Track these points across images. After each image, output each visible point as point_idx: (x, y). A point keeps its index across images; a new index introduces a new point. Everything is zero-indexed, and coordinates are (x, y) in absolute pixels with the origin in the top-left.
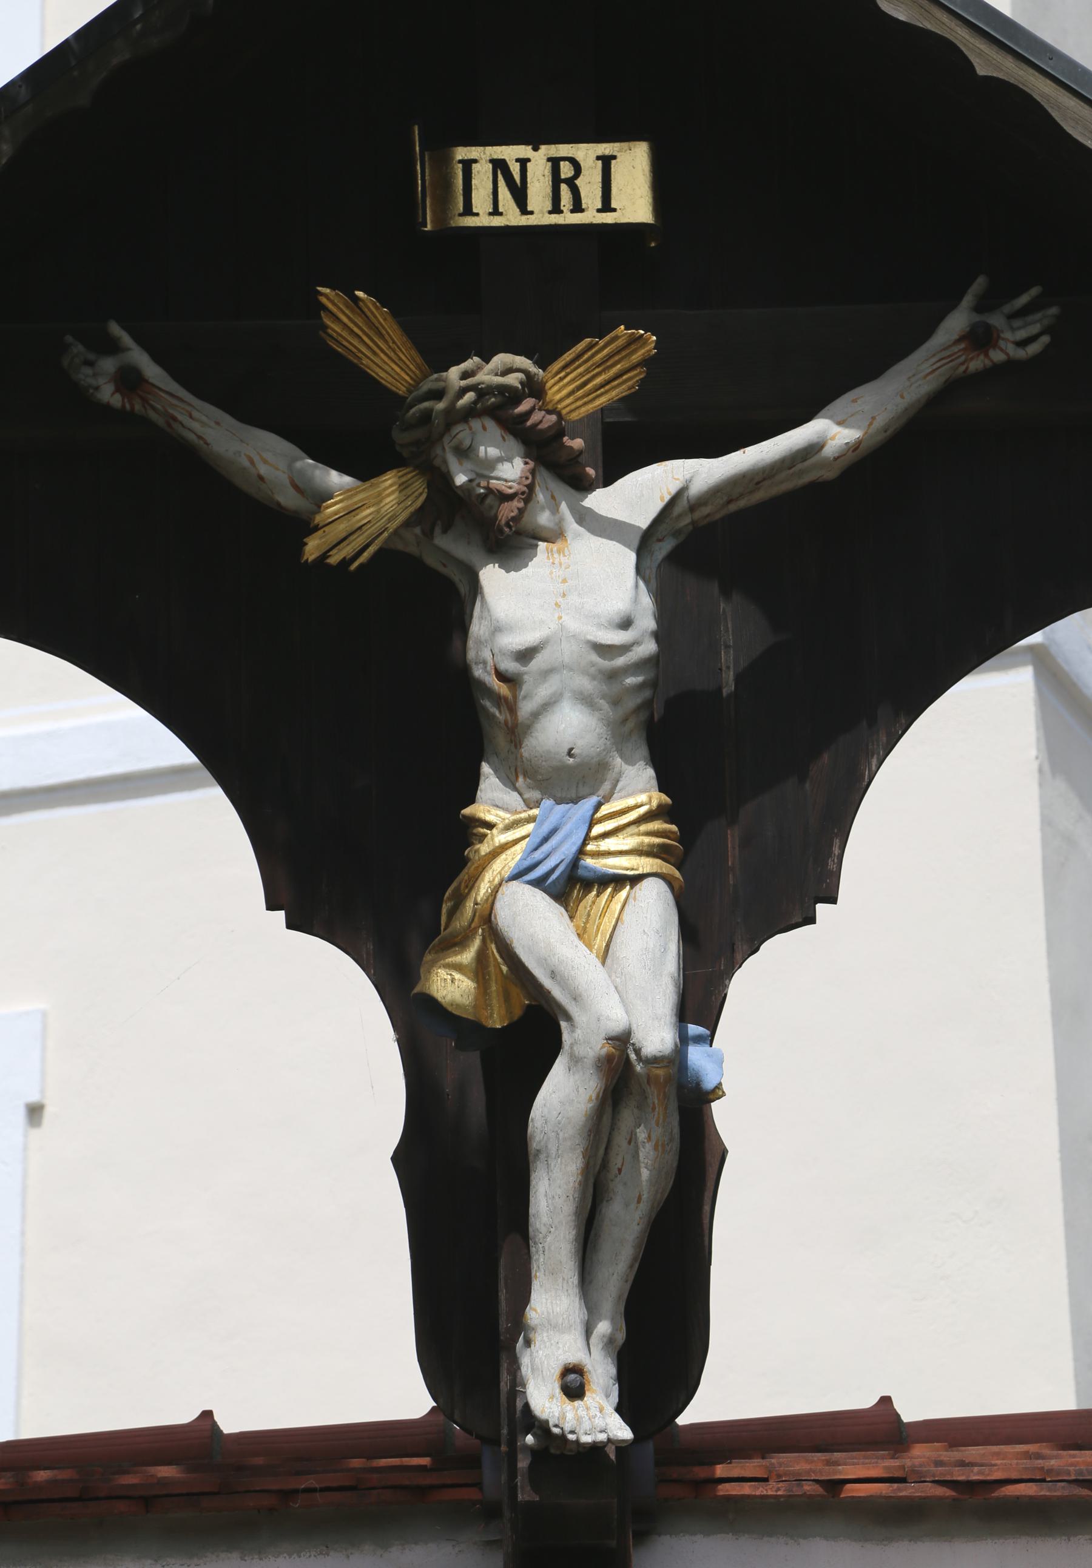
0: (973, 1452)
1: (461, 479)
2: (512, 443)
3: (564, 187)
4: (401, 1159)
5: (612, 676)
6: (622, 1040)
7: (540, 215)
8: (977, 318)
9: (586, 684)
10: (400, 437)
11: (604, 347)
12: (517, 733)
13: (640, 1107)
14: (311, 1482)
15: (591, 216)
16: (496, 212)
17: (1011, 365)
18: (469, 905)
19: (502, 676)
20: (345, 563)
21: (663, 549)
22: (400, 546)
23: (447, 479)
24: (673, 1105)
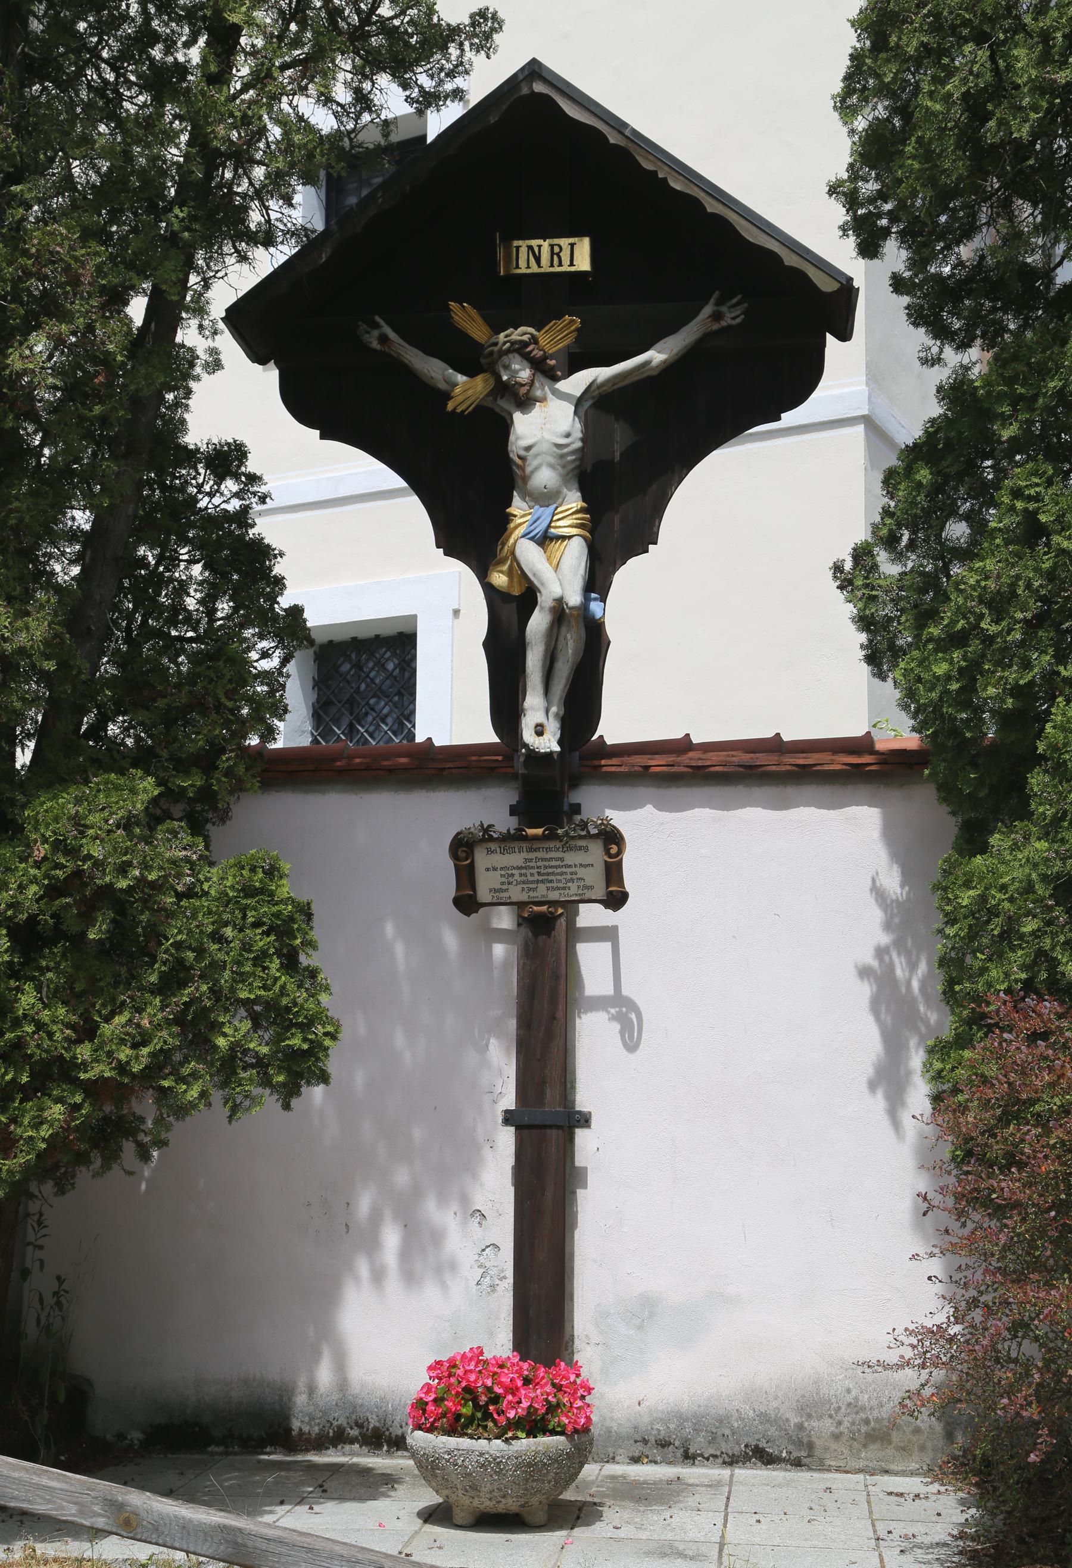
0: (709, 755)
1: (505, 378)
2: (525, 363)
3: (555, 257)
4: (487, 645)
5: (562, 456)
6: (560, 601)
7: (545, 268)
8: (716, 308)
9: (551, 460)
10: (483, 361)
11: (560, 324)
12: (525, 479)
13: (568, 626)
14: (451, 765)
15: (566, 268)
16: (528, 267)
17: (729, 327)
18: (506, 547)
19: (520, 457)
20: (463, 411)
21: (587, 404)
22: (485, 404)
23: (500, 377)
24: (582, 625)
